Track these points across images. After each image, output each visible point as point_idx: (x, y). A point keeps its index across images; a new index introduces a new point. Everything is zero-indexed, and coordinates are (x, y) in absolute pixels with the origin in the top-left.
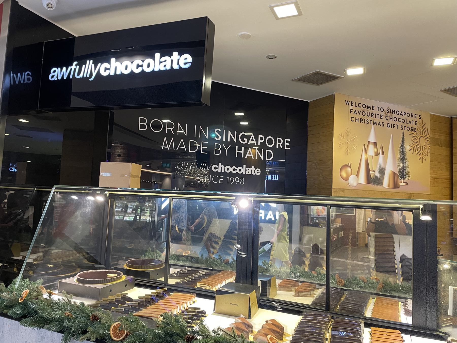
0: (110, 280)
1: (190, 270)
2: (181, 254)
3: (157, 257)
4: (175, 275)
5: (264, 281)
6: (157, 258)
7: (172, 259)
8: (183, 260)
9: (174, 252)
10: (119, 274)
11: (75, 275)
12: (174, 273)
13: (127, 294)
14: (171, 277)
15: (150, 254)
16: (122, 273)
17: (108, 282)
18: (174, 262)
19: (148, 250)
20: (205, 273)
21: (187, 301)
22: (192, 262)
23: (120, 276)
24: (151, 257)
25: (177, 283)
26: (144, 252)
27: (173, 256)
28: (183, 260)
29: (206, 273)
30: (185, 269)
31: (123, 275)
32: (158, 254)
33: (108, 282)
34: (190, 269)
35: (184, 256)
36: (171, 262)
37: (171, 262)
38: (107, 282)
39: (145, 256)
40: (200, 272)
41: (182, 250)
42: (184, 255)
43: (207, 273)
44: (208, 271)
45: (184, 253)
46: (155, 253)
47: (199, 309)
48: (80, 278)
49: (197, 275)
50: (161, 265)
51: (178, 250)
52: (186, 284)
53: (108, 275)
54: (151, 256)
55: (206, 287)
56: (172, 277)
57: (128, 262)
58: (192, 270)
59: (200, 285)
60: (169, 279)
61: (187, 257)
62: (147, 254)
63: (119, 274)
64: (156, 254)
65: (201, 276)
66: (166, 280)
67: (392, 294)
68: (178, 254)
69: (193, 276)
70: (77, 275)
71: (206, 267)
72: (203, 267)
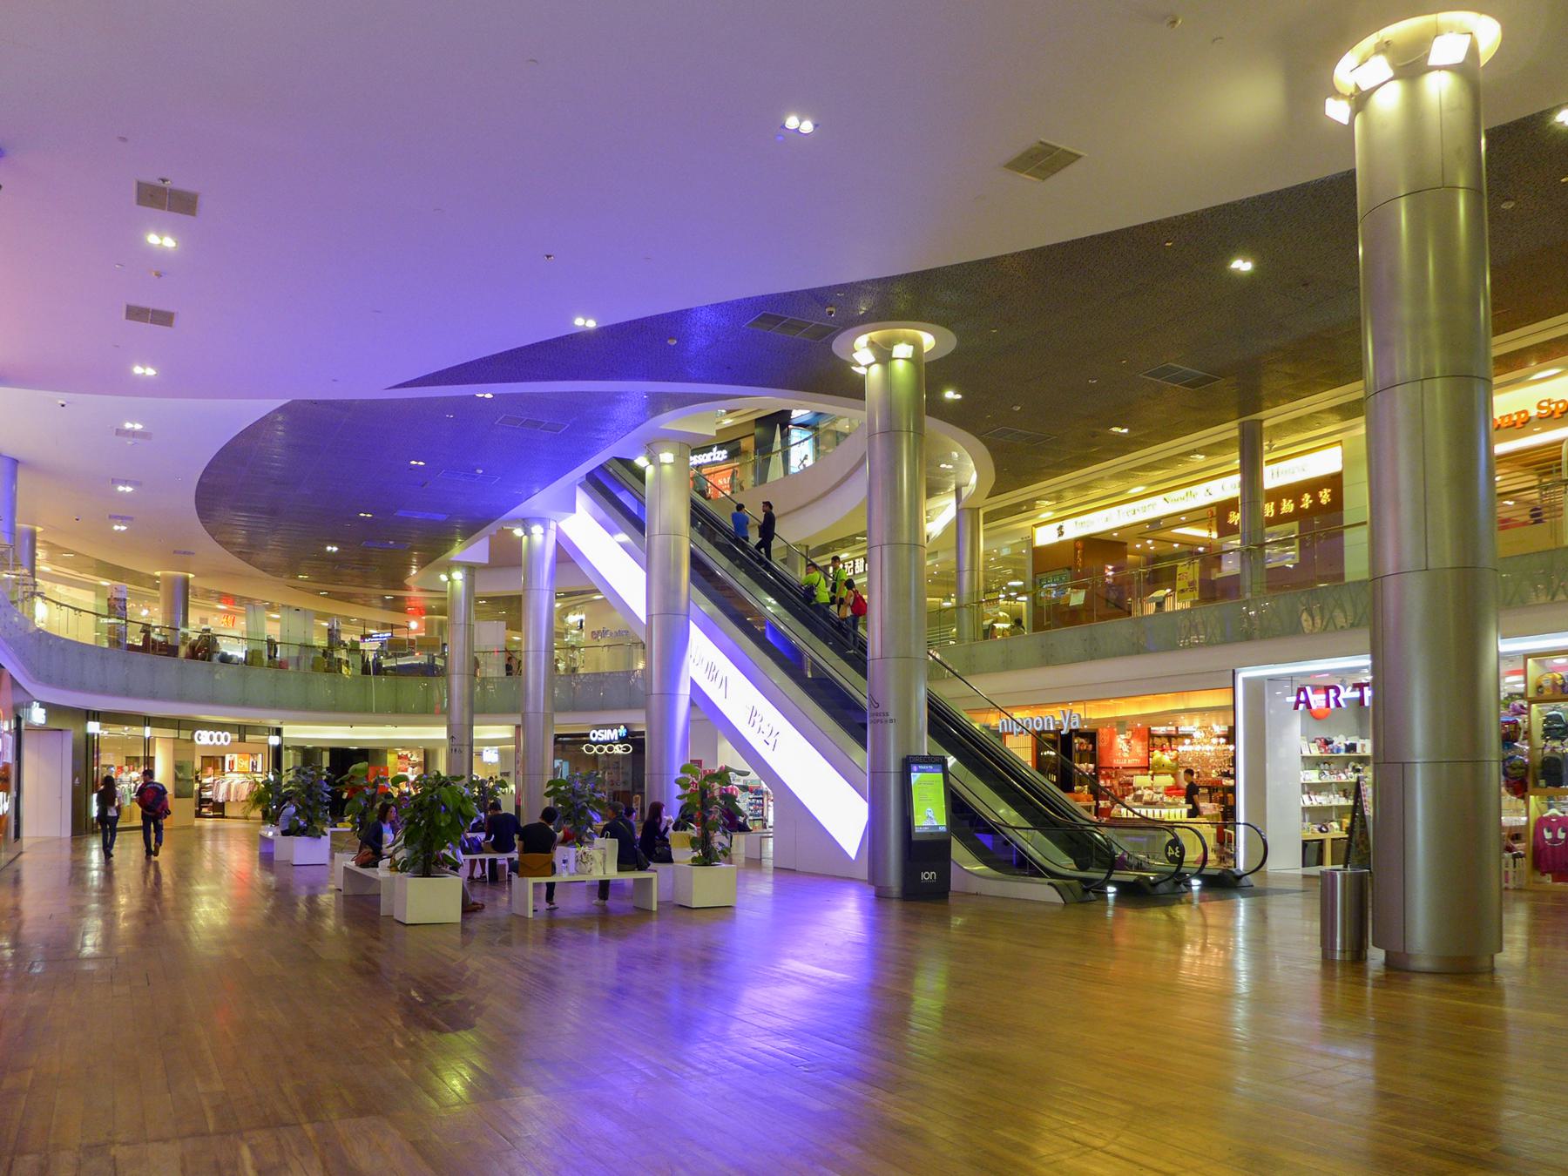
5: (1332, 858)
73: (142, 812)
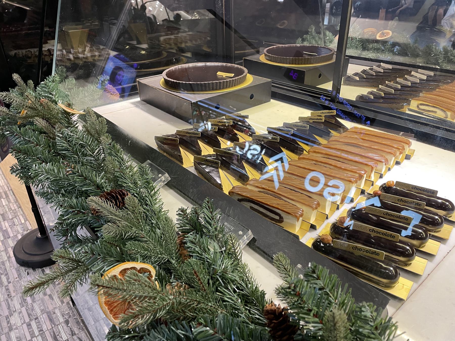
0: (223, 85)
1: (390, 69)
2: (372, 38)
3: (325, 42)
4: (357, 78)
6: (325, 46)
7: (352, 47)
8: (375, 49)
9: (358, 34)
10: (239, 72)
11: (160, 72)
12: (356, 74)
13: (247, 117)
14: (347, 82)
15: (313, 38)
16: (246, 70)
17: (226, 86)
18: (356, 53)
19: (310, 30)
20: (425, 78)
21: (388, 157)
22: (394, 54)
23: (242, 76)
24: (314, 42)
25: (361, 98)
26: (303, 33)
27: (356, 41)
28: (375, 49)
29: (428, 76)
30: (379, 66)
31: (248, 73)
32: (328, 38)
33: (226, 86)
34: (390, 67)
35: (377, 41)
36: (350, 52)
37: (350, 52)
38: (222, 87)
39: (303, 40)
40: (413, 73)
41: (374, 30)
42: (378, 38)
43: (431, 76)
44: (432, 74)
45: (378, 35)
46: (322, 36)
47: (434, 193)
48: (168, 79)
49: (406, 79)
50: (330, 58)
51: (366, 31)
52: (382, 101)
53: (219, 73)
54: (316, 41)
55: (436, 112)
56: (350, 81)
57: (268, 51)
58: (393, 69)
59: (418, 107)
60: (344, 84)
61: (384, 42)
62: (308, 37)
63: (239, 72)
64: (324, 38)
65: (416, 83)
66: (337, 89)
67: (175, 36)
68: (366, 37)
69: (397, 83)
70: (165, 73)
71: (424, 63)
72: (418, 64)
73: (181, 153)
